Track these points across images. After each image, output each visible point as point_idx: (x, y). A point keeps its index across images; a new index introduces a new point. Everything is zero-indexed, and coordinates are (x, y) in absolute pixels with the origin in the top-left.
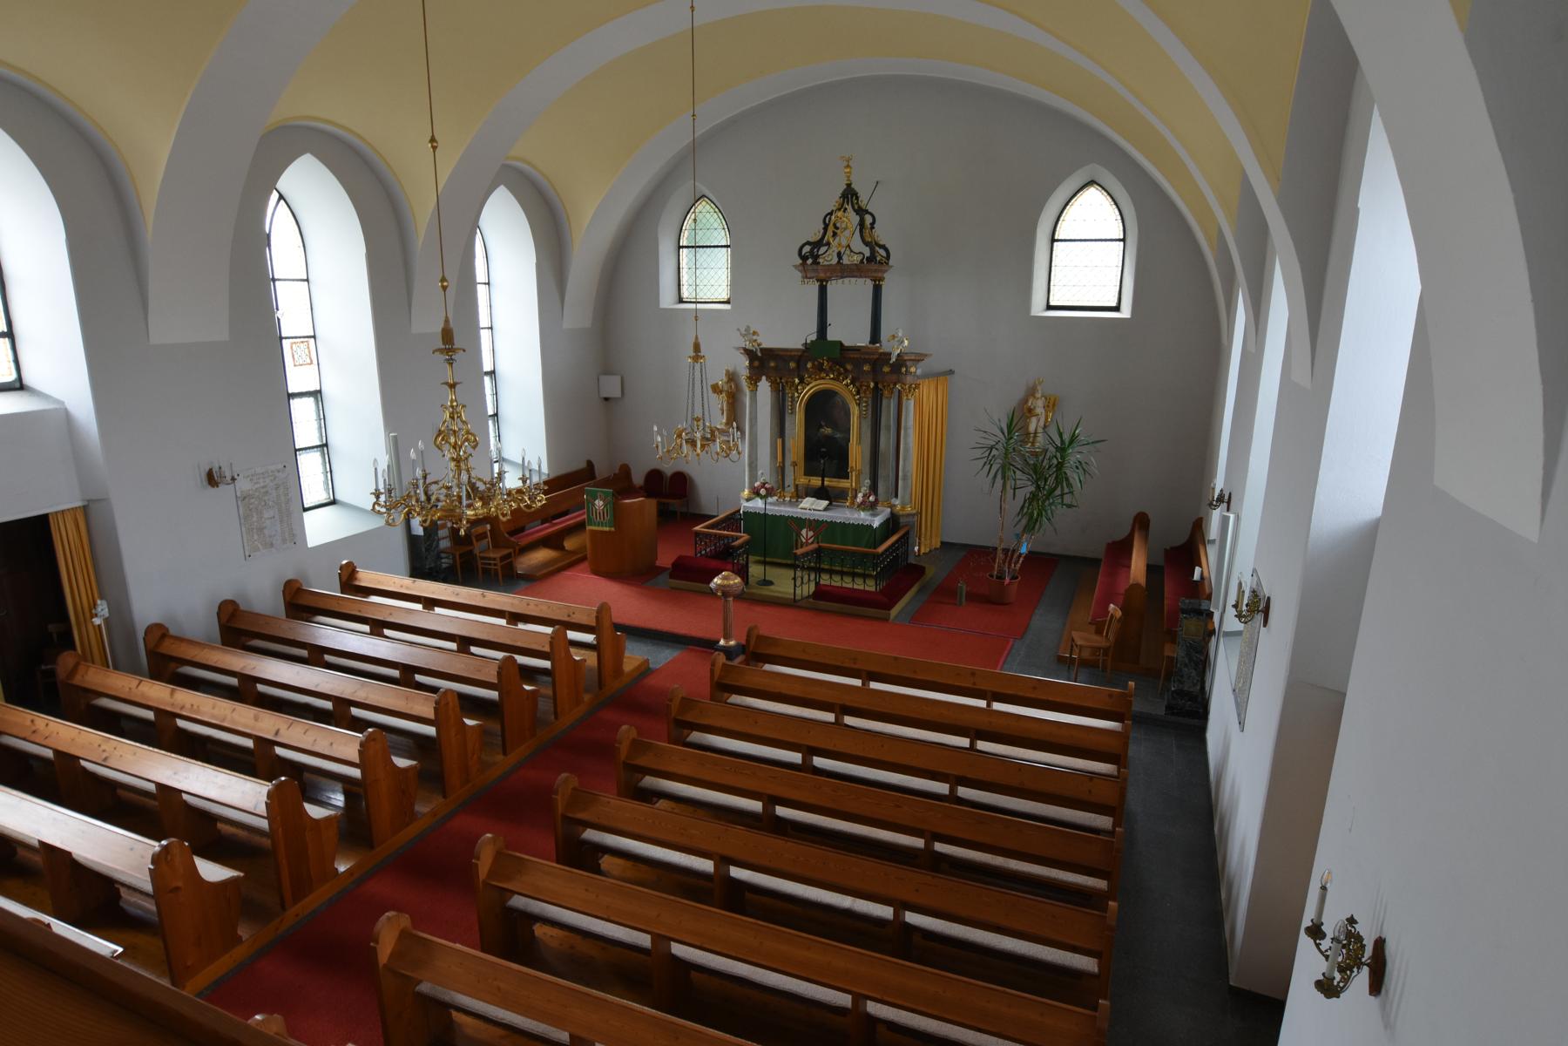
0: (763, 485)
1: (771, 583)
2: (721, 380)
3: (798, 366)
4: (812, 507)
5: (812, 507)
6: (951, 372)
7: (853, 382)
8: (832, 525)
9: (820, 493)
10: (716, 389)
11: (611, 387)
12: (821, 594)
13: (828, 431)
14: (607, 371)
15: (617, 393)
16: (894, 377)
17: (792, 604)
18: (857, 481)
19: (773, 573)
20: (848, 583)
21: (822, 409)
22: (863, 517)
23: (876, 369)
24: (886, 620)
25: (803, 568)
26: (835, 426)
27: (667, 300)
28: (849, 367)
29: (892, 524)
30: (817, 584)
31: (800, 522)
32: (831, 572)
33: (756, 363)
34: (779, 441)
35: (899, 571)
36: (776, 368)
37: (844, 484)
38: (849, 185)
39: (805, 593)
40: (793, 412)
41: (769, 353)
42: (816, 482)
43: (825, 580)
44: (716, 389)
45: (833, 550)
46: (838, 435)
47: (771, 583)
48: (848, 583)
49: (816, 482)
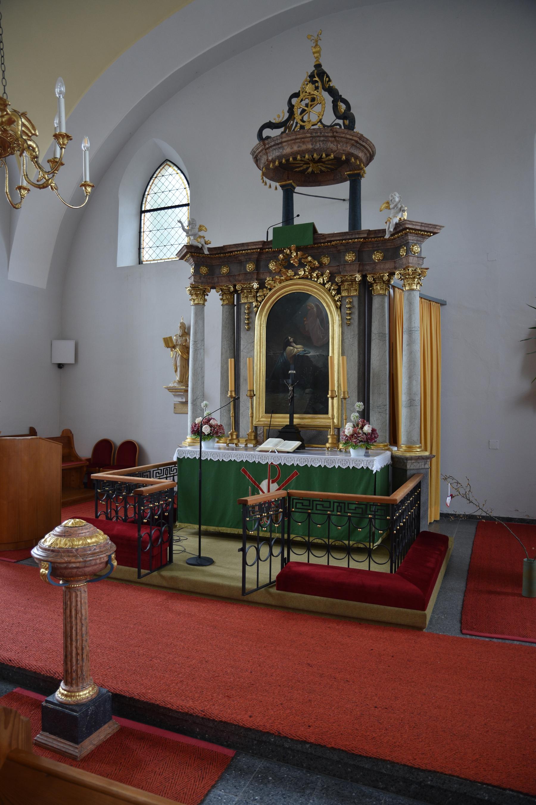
0: (207, 421)
1: (209, 562)
2: (175, 333)
3: (257, 268)
4: (278, 450)
5: (278, 450)
6: (443, 304)
7: (331, 279)
8: (307, 473)
9: (287, 433)
10: (168, 343)
11: (64, 352)
12: (291, 579)
13: (297, 349)
14: (62, 336)
15: (69, 359)
16: (389, 265)
17: (239, 597)
18: (339, 412)
19: (211, 547)
20: (339, 561)
21: (291, 321)
22: (354, 457)
23: (362, 261)
24: (416, 628)
25: (267, 541)
26: (306, 339)
27: (125, 258)
28: (326, 260)
29: (397, 471)
30: (285, 561)
31: (257, 471)
32: (309, 547)
33: (204, 270)
34: (231, 362)
35: (418, 549)
36: (229, 275)
37: (319, 420)
38: (318, 66)
39: (264, 579)
40: (250, 327)
41: (224, 254)
42: (282, 420)
43: (298, 556)
44: (168, 343)
45: (311, 501)
46: (312, 353)
47: (209, 562)
48: (339, 561)
49: (282, 420)
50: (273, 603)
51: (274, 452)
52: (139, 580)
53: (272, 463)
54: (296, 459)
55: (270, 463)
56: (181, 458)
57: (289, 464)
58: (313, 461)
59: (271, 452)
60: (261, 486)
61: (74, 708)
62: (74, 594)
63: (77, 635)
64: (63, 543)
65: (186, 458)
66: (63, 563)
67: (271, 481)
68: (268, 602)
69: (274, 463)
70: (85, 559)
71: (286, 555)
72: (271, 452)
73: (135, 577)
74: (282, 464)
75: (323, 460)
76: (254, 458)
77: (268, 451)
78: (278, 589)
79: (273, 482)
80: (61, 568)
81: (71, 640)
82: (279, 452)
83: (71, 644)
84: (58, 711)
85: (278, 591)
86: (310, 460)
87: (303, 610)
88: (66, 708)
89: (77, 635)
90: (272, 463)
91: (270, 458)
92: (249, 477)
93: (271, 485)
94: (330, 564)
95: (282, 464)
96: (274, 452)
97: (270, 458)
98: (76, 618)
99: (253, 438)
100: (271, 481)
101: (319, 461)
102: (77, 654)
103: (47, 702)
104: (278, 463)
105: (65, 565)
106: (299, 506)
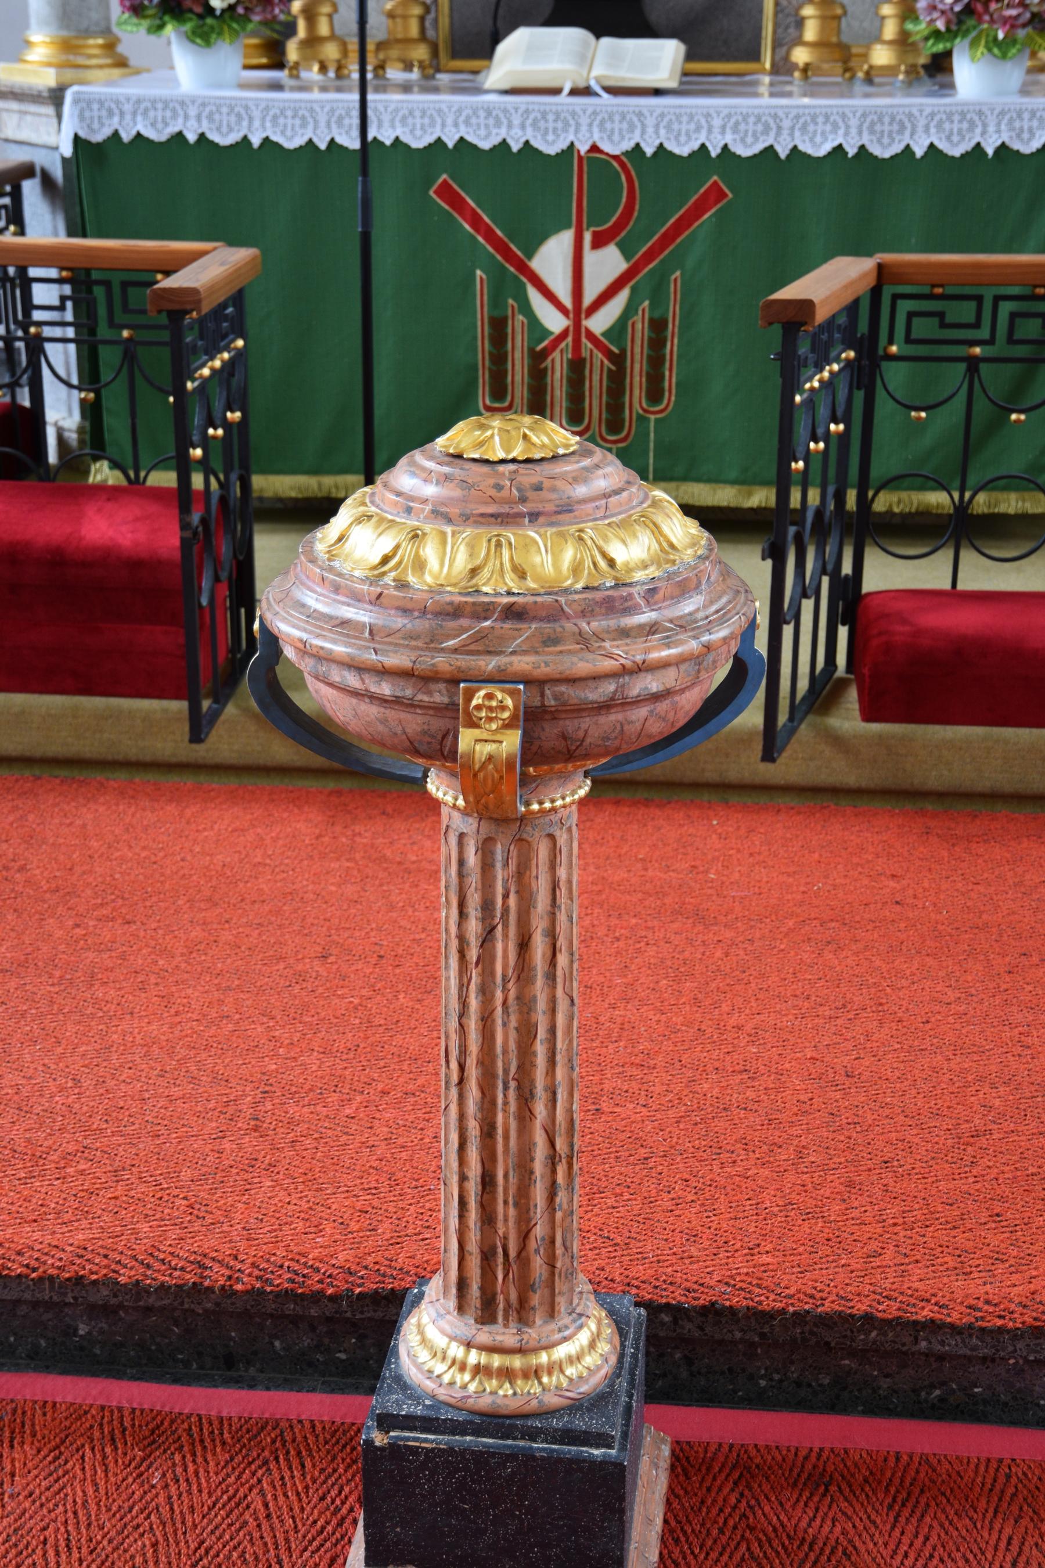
31: (527, 188)
50: (852, 779)
51: (585, 91)
52: (201, 752)
53: (594, 148)
54: (717, 122)
55: (583, 148)
56: (98, 137)
57: (683, 149)
58: (804, 129)
59: (574, 92)
60: (536, 264)
61: (580, 1424)
62: (543, 851)
63: (552, 1061)
64: (445, 562)
65: (126, 137)
66: (597, 677)
67: (588, 237)
68: (824, 778)
69: (607, 147)
70: (705, 638)
71: (847, 569)
72: (574, 92)
73: (174, 743)
74: (649, 151)
75: (854, 122)
76: (498, 124)
77: (556, 91)
78: (870, 714)
79: (598, 243)
80: (581, 710)
81: (526, 1098)
82: (614, 91)
83: (525, 1113)
84: (482, 1457)
85: (875, 727)
86: (786, 124)
87: (993, 797)
88: (532, 1435)
89: (552, 1061)
90: (594, 148)
91: (584, 121)
92: (476, 221)
93: (590, 257)
94: (960, 587)
95: (649, 151)
96: (585, 91)
97: (584, 121)
98: (551, 977)
99: (414, 31)
100: (588, 237)
101: (835, 127)
102: (553, 1160)
103: (386, 1422)
104: (627, 145)
105: (610, 687)
106: (923, 328)
